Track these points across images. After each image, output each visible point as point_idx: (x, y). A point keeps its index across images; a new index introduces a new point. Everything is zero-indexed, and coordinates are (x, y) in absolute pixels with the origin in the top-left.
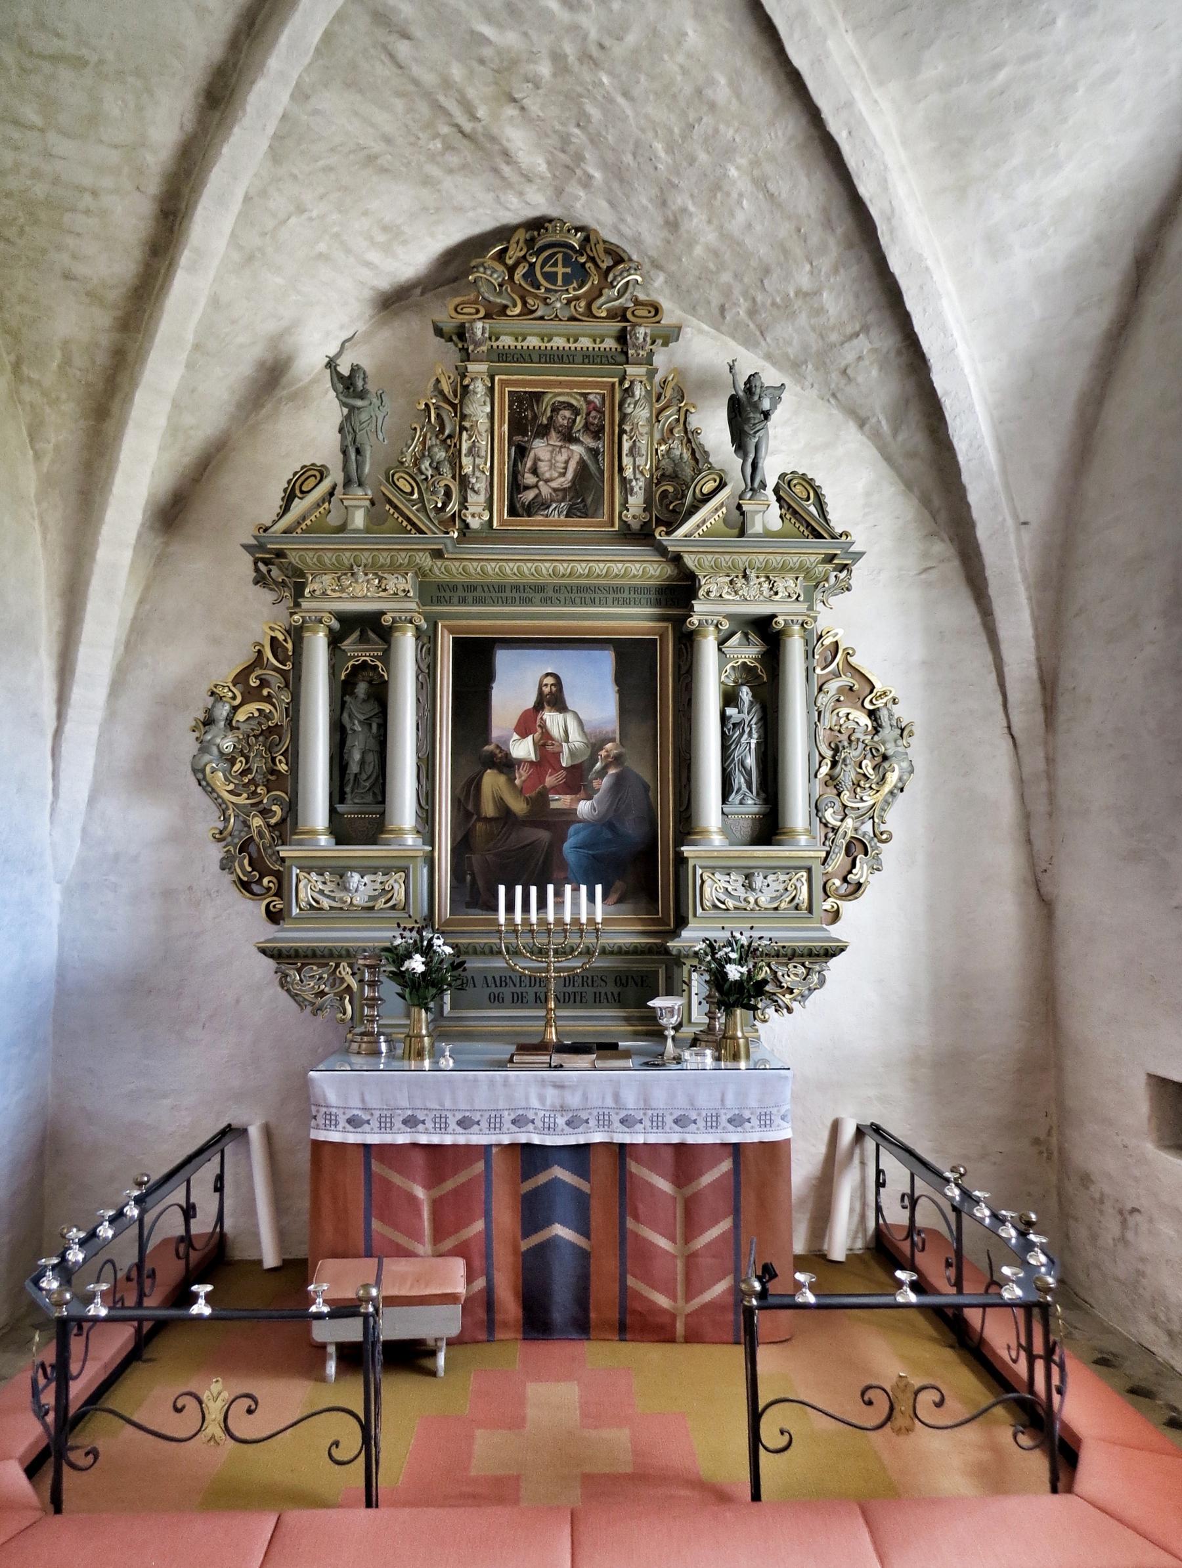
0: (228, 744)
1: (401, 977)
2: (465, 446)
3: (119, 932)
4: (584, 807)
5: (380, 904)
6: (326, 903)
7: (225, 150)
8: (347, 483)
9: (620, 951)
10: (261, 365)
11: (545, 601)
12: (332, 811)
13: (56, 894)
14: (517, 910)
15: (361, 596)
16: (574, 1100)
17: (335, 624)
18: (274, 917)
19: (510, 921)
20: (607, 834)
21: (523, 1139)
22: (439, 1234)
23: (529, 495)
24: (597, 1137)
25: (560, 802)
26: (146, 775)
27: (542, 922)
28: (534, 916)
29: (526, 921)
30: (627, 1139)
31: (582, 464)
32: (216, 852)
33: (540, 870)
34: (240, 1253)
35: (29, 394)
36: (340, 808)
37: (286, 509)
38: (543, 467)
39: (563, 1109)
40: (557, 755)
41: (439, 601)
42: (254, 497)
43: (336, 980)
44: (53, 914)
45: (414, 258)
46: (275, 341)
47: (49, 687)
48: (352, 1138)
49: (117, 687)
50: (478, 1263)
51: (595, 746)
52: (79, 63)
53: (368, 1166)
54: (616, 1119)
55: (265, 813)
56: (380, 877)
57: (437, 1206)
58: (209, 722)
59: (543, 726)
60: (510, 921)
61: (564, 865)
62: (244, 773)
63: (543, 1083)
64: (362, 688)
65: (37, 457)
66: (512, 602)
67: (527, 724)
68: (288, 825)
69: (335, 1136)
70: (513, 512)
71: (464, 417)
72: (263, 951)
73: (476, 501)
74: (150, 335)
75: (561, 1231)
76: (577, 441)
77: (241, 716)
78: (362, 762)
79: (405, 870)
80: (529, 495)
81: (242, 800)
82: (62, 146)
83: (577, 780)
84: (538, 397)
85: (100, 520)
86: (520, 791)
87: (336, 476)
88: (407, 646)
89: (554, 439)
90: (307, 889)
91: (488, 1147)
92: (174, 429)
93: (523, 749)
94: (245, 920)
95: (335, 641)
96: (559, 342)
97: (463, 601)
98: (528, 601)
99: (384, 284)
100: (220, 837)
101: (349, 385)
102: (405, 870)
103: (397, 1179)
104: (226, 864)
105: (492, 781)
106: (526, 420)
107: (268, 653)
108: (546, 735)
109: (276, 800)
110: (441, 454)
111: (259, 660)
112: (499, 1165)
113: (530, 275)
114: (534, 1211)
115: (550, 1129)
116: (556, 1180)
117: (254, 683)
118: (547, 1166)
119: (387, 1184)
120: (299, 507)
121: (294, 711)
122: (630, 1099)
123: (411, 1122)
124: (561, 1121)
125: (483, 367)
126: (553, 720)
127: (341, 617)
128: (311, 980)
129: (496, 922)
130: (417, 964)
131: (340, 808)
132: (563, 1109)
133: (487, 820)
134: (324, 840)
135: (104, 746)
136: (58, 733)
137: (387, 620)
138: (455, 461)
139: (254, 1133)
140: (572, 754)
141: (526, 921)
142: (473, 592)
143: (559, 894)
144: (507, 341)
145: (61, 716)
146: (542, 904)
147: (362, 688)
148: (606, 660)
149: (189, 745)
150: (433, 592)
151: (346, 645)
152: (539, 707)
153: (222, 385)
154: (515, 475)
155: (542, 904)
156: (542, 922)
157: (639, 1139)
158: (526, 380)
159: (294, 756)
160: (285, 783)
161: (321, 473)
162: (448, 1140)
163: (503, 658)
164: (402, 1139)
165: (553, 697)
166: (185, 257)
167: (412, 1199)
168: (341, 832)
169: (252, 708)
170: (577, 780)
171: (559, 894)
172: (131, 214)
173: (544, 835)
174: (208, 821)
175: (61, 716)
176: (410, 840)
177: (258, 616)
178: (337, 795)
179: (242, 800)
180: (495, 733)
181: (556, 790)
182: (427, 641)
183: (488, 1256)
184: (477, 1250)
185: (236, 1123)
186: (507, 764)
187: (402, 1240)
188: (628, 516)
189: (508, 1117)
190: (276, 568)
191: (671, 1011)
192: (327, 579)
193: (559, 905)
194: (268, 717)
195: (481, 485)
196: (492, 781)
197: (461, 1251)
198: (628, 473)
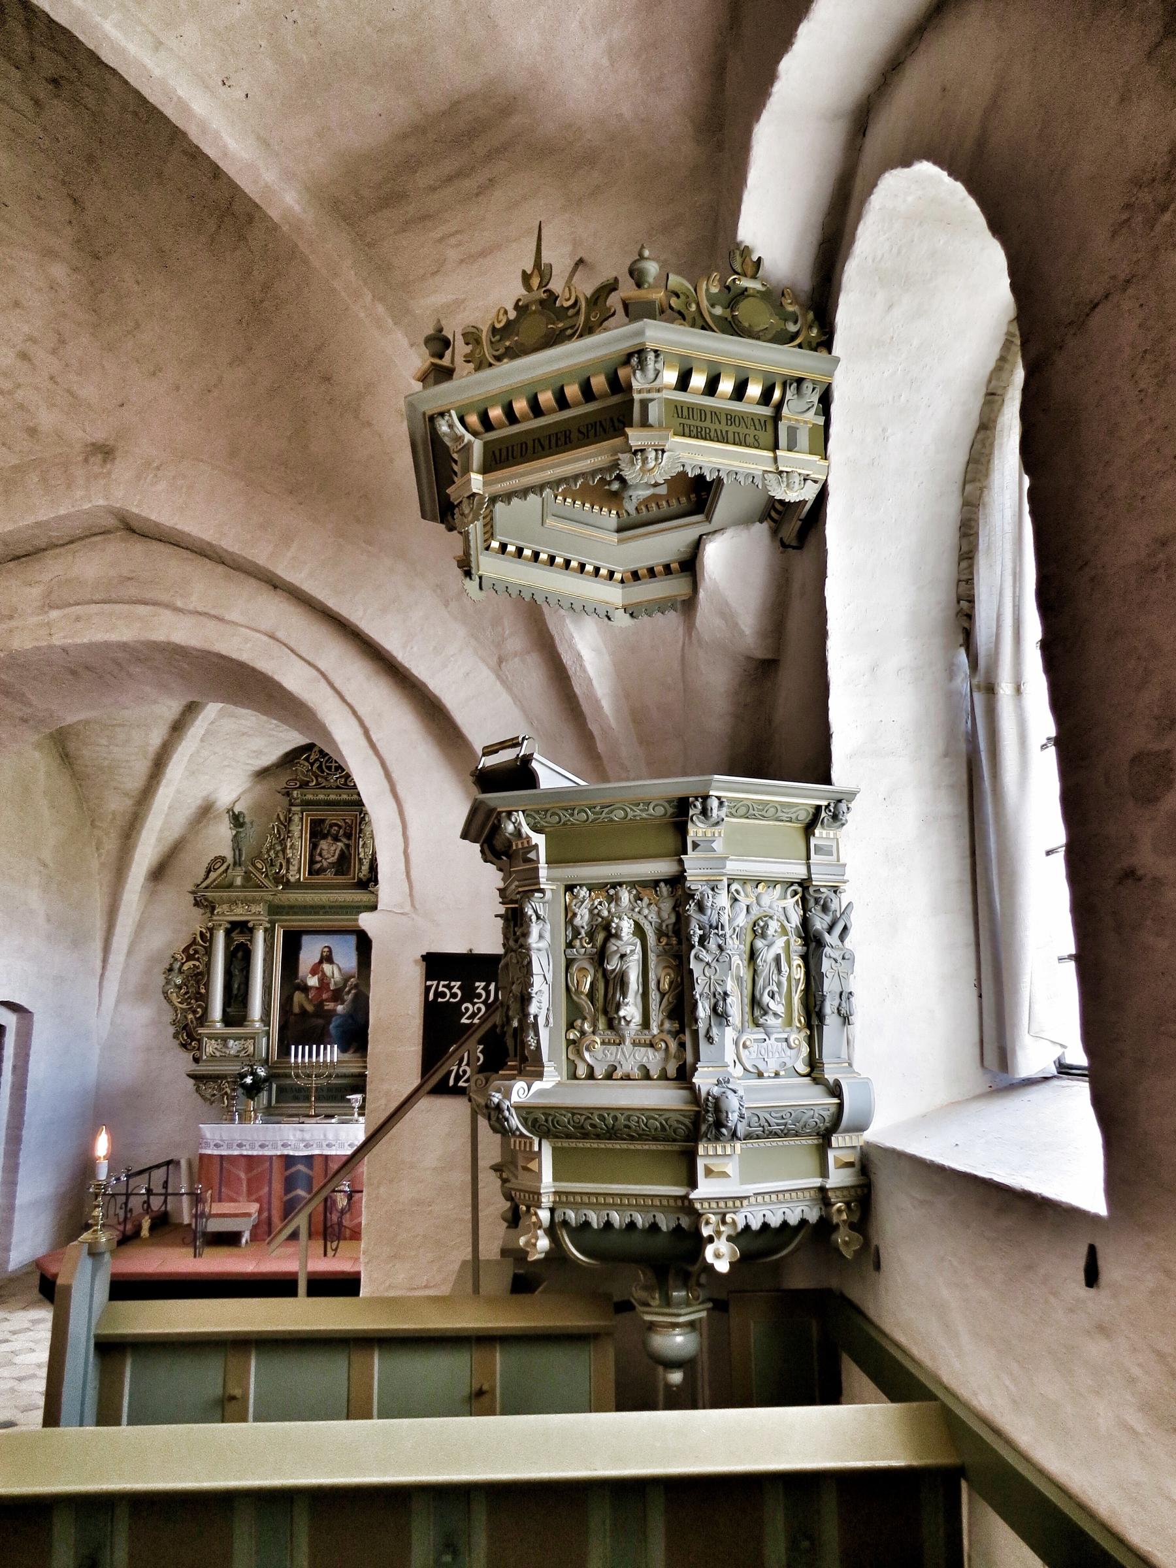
0: (179, 981)
1: (244, 1086)
2: (289, 845)
3: (128, 1067)
4: (340, 1008)
5: (242, 1054)
6: (218, 1054)
7: (180, 749)
8: (235, 864)
9: (345, 1076)
10: (200, 807)
11: (326, 913)
12: (224, 1011)
13: (97, 1051)
14: (299, 1055)
15: (239, 913)
16: (307, 1136)
17: (228, 926)
18: (196, 1060)
19: (296, 1062)
20: (350, 1021)
21: (286, 1153)
22: (250, 1193)
23: (318, 866)
24: (317, 1152)
25: (329, 1006)
26: (142, 994)
27: (318, 1062)
28: (314, 1059)
29: (303, 1062)
30: (329, 1153)
31: (342, 850)
32: (172, 1030)
33: (317, 1037)
34: (175, 1220)
35: (97, 832)
36: (228, 1010)
37: (207, 877)
38: (324, 853)
39: (303, 1140)
40: (328, 984)
41: (277, 914)
42: (193, 867)
43: (220, 1089)
44: (95, 1059)
45: (272, 756)
46: (206, 799)
47: (99, 955)
48: (216, 1152)
49: (130, 953)
50: (265, 1206)
51: (346, 980)
52: (124, 726)
53: (222, 1164)
54: (324, 1144)
55: (195, 1012)
56: (242, 1042)
57: (249, 1181)
58: (170, 970)
59: (323, 971)
60: (296, 1062)
61: (329, 1035)
62: (186, 993)
63: (295, 1129)
64: (240, 954)
65: (100, 856)
66: (310, 914)
67: (315, 970)
68: (203, 1020)
69: (209, 1152)
70: (310, 874)
71: (289, 832)
72: (189, 1075)
73: (293, 868)
74: (149, 809)
75: (301, 1192)
76: (340, 841)
77: (185, 967)
78: (239, 988)
79: (254, 1038)
80: (318, 866)
81: (184, 1006)
82: (116, 749)
83: (337, 996)
84: (323, 821)
85: (125, 882)
86: (310, 1001)
87: (230, 860)
88: (260, 936)
89: (330, 840)
90: (210, 1047)
91: (271, 1157)
92: (159, 840)
93: (313, 981)
94: (183, 1061)
95: (228, 933)
96: (332, 797)
97: (288, 914)
98: (317, 913)
99: (257, 768)
100: (174, 1023)
101: (237, 820)
102: (254, 1038)
103: (234, 1170)
104: (175, 1036)
105: (298, 997)
106: (317, 832)
107: (199, 939)
108: (324, 974)
109: (199, 1006)
110: (279, 848)
111: (194, 942)
112: (276, 1165)
113: (320, 767)
114: (289, 1184)
115: (296, 1149)
116: (299, 1171)
117: (191, 952)
118: (294, 1164)
119: (229, 1172)
120: (213, 875)
121: (209, 965)
122: (331, 1136)
123: (240, 1146)
124: (302, 1145)
125: (299, 808)
126: (327, 968)
127: (231, 923)
128: (209, 1089)
129: (289, 1062)
130: (249, 1080)
131: (228, 1010)
132: (303, 1140)
133: (296, 1015)
134: (219, 1025)
135: (123, 981)
136: (102, 975)
137: (250, 925)
138: (284, 851)
139: (183, 1163)
140: (335, 984)
141: (303, 1062)
142: (293, 909)
143: (325, 1049)
144: (310, 797)
145: (104, 968)
146: (310, 1055)
147: (240, 954)
148: (488, 940)
149: (161, 980)
150: (275, 910)
151: (233, 935)
152: (321, 962)
153: (181, 819)
154: (311, 856)
155: (310, 1055)
156: (318, 1062)
157: (333, 1153)
158: (319, 815)
159: (207, 986)
160: (204, 999)
161: (223, 859)
162: (255, 1153)
163: (306, 940)
164: (236, 1153)
165: (328, 958)
166: (164, 782)
167: (239, 1179)
168: (227, 1021)
169: (191, 963)
170: (337, 996)
171: (325, 1049)
172: (141, 768)
173: (320, 1021)
174: (169, 1016)
175: (104, 968)
176: (257, 1025)
177: (196, 921)
178: (227, 1003)
179: (184, 1006)
180: (300, 974)
181: (326, 1000)
182: (270, 933)
183: (270, 1203)
184: (265, 1200)
185: (175, 1158)
186: (305, 989)
187: (235, 1196)
188: (361, 875)
189: (280, 1143)
190: (204, 903)
191: (356, 1100)
192: (225, 907)
193: (325, 1054)
194: (198, 967)
195: (295, 862)
196: (298, 997)
197: (257, 1200)
198: (362, 856)
